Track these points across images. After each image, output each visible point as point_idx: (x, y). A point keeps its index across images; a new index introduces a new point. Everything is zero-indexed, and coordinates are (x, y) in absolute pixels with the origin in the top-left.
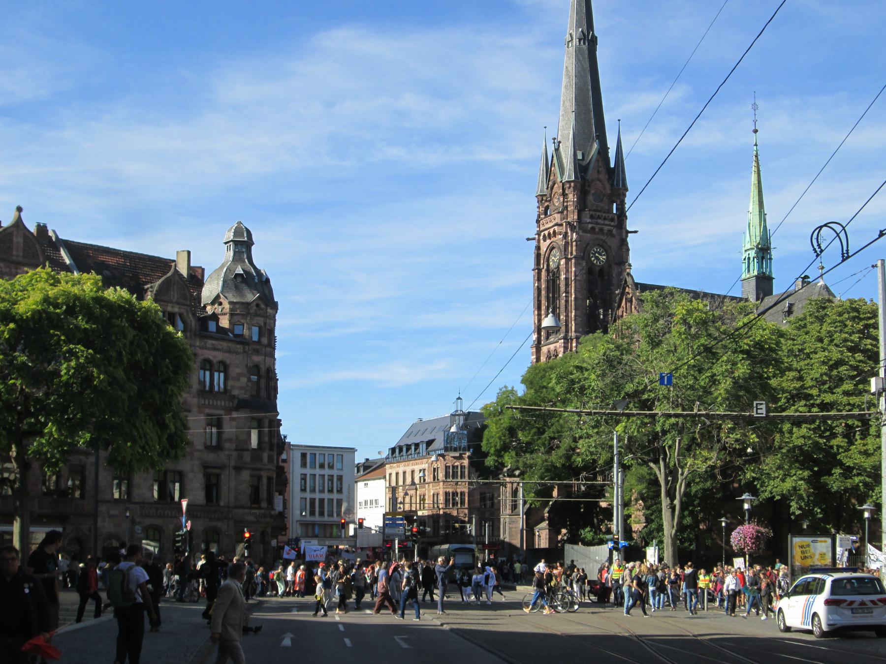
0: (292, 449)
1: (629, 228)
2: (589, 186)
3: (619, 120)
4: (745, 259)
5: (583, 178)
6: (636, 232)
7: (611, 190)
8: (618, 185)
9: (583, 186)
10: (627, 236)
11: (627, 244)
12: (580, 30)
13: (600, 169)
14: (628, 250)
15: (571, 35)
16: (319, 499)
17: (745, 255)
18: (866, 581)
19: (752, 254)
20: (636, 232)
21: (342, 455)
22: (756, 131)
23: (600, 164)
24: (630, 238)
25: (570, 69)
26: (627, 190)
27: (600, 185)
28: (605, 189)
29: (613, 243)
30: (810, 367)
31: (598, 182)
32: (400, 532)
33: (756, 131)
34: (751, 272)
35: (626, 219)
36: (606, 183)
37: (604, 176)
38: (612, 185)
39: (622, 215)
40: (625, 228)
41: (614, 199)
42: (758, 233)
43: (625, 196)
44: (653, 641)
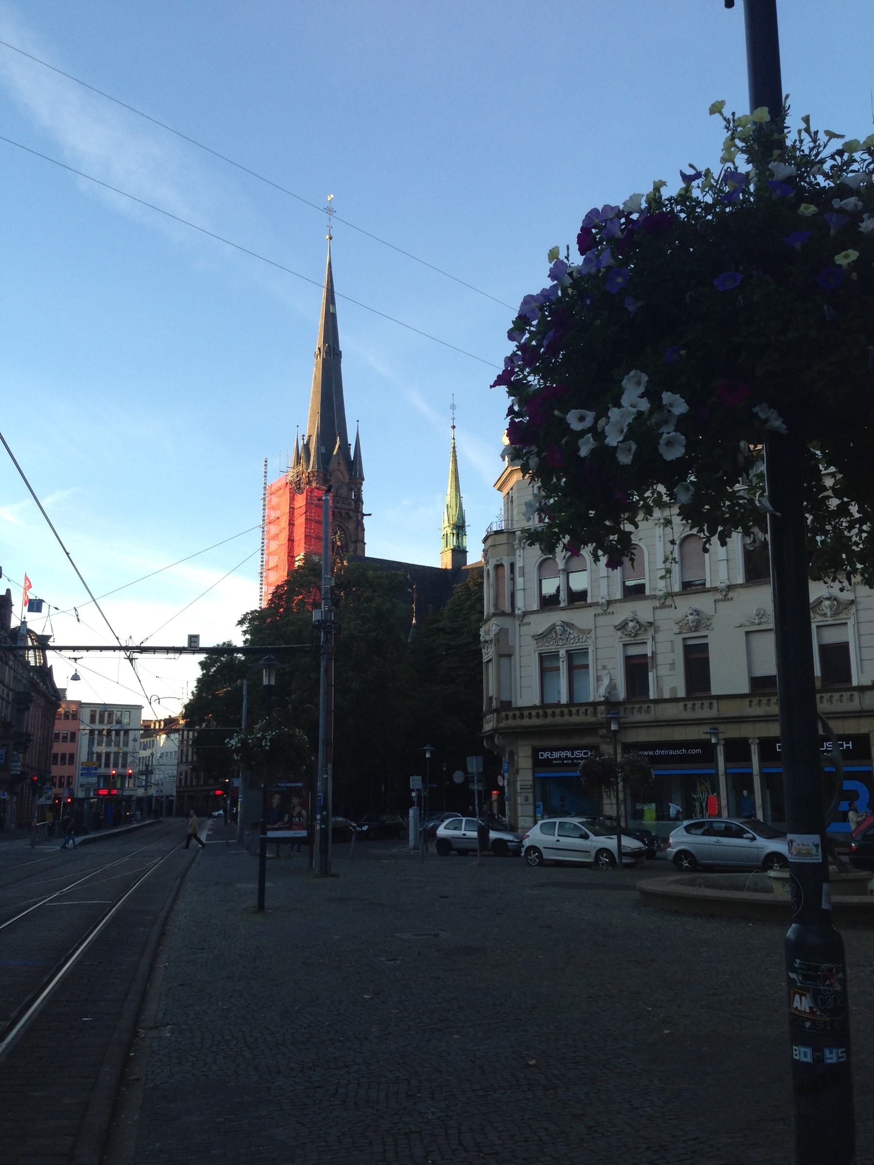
0: (82, 707)
1: (364, 512)
2: (331, 476)
3: (358, 421)
4: (444, 535)
5: (325, 469)
6: (370, 515)
7: (350, 479)
8: (356, 475)
9: (325, 475)
10: (363, 519)
11: (362, 525)
12: (327, 345)
13: (340, 461)
14: (363, 530)
15: (319, 349)
16: (70, 754)
17: (444, 532)
18: (745, 792)
19: (449, 530)
20: (370, 515)
21: (130, 712)
22: (454, 427)
23: (341, 456)
24: (366, 520)
25: (317, 378)
26: (363, 479)
27: (341, 475)
28: (344, 478)
29: (351, 526)
30: (681, 624)
31: (338, 473)
32: (94, 781)
33: (454, 427)
34: (449, 546)
35: (363, 504)
36: (346, 474)
37: (343, 468)
38: (350, 475)
39: (359, 501)
40: (361, 512)
41: (353, 486)
42: (454, 513)
43: (361, 484)
44: (80, 886)
